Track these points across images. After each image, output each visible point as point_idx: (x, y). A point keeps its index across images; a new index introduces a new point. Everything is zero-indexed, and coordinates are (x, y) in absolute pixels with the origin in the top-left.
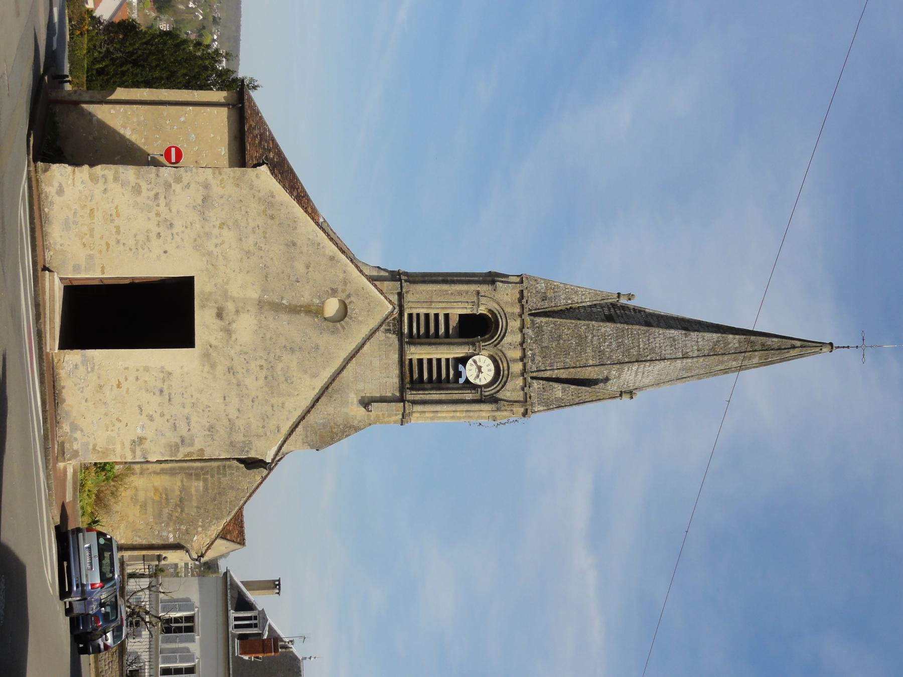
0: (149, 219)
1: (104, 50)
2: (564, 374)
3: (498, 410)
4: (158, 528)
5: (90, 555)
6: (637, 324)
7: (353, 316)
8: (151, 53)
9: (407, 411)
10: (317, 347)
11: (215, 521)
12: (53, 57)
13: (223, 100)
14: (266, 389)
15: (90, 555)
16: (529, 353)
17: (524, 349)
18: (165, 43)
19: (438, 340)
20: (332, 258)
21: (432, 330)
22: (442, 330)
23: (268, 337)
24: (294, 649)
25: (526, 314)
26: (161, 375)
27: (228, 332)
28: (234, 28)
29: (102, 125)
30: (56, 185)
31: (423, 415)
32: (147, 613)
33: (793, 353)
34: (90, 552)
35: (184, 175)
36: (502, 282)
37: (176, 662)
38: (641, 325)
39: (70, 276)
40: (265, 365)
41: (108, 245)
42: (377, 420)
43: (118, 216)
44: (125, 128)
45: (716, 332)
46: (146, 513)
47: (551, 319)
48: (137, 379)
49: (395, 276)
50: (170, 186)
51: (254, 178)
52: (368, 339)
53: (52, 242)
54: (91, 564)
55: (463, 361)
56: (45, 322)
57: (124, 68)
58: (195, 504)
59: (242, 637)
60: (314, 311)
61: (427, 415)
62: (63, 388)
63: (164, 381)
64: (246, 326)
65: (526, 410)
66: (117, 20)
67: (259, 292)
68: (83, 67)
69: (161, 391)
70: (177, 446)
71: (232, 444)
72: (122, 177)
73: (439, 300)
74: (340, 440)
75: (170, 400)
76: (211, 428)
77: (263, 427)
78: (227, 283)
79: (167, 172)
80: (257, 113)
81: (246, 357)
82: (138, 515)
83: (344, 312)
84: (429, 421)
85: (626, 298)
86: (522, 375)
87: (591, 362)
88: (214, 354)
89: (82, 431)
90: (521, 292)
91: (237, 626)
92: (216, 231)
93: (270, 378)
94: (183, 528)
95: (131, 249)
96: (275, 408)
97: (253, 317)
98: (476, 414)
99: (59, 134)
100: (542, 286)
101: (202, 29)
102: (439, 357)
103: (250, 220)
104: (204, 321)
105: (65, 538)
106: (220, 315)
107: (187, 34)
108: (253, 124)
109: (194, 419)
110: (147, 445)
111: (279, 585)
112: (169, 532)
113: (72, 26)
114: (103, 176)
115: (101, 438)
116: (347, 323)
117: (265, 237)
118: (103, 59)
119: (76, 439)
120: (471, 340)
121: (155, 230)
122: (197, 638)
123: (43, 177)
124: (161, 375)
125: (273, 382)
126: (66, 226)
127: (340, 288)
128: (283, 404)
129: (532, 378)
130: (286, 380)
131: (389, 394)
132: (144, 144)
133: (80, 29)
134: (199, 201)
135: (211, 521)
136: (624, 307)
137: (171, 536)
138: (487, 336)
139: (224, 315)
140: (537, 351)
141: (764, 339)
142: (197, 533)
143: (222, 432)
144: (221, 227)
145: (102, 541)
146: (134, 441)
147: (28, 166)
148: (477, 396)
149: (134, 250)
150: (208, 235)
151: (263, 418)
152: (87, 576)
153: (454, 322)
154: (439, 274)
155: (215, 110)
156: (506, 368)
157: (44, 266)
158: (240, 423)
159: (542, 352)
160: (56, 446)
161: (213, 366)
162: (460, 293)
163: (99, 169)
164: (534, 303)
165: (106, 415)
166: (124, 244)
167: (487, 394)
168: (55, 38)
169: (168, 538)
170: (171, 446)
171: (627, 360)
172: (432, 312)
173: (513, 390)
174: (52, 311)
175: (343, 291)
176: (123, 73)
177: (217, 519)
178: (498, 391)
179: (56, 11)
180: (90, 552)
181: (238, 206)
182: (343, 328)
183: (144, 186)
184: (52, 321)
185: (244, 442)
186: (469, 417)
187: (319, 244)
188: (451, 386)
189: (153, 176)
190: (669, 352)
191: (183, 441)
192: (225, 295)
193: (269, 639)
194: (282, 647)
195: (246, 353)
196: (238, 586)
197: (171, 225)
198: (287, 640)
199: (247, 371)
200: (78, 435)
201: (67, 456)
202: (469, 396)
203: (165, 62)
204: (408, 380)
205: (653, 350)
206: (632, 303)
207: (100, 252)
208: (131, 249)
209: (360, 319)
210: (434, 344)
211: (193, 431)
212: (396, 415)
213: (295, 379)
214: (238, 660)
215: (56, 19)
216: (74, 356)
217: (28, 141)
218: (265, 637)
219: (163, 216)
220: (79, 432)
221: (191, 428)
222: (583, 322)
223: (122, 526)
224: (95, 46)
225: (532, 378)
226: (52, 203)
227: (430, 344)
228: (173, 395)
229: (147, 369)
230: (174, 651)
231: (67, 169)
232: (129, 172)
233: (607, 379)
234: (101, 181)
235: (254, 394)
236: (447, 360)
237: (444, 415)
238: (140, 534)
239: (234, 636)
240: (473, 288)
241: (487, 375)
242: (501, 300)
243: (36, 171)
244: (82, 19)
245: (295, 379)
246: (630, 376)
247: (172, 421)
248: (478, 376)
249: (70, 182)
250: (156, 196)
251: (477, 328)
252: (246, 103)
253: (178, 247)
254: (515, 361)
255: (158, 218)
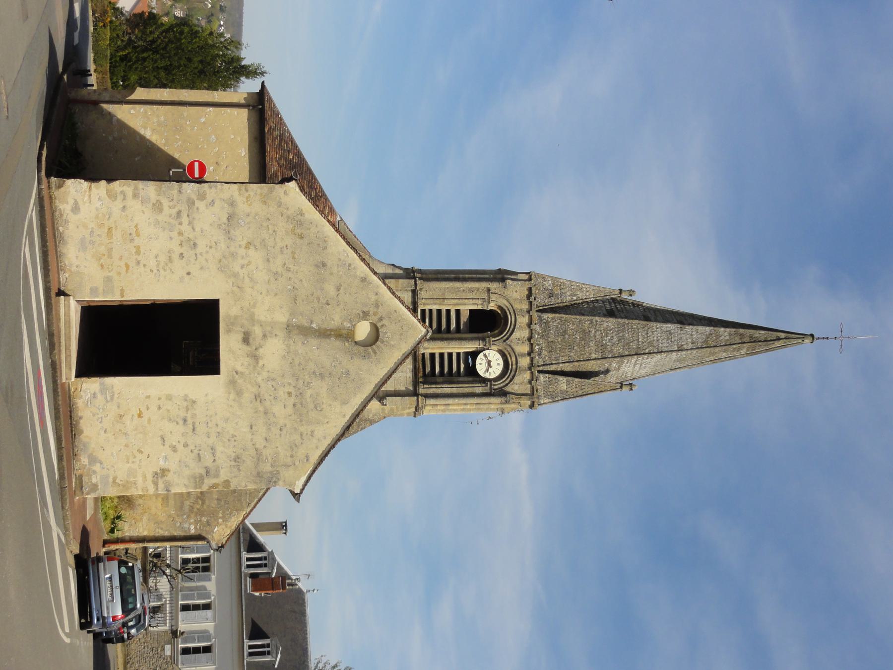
0: (171, 238)
1: (126, 38)
2: (568, 368)
3: (507, 402)
4: (180, 520)
5: (112, 586)
6: (636, 319)
7: (385, 339)
8: (170, 41)
9: (420, 405)
10: (348, 373)
11: (235, 512)
12: (74, 53)
13: (243, 101)
14: (294, 417)
15: (112, 586)
16: (536, 348)
17: (532, 345)
18: (181, 33)
19: (450, 336)
20: (364, 280)
21: (444, 326)
22: (453, 326)
23: (297, 362)
24: (300, 585)
25: (534, 310)
26: (185, 404)
27: (255, 358)
28: (237, 16)
29: (122, 125)
30: (71, 201)
31: (435, 408)
32: (168, 566)
33: (777, 344)
34: (111, 583)
35: (208, 191)
36: (512, 279)
37: (194, 599)
38: (640, 319)
39: (86, 299)
40: (293, 393)
41: (127, 266)
42: (392, 413)
43: (138, 235)
44: (146, 128)
45: (709, 325)
46: (167, 506)
47: (557, 315)
48: (159, 408)
49: (410, 274)
50: (193, 203)
51: (282, 194)
52: (401, 364)
53: (67, 263)
54: (112, 595)
55: (474, 355)
56: (60, 351)
57: (145, 55)
58: (215, 496)
59: (253, 576)
60: (345, 335)
61: (439, 407)
62: (81, 418)
63: (187, 410)
64: (273, 351)
65: (533, 403)
66: (138, 11)
67: (287, 316)
68: (106, 56)
69: (185, 421)
70: (201, 478)
71: (259, 475)
72: (142, 193)
73: (451, 296)
74: (355, 433)
75: (194, 430)
76: (237, 459)
77: (292, 456)
78: (254, 306)
79: (189, 188)
80: (278, 114)
81: (273, 383)
82: (160, 507)
83: (375, 336)
84: (440, 413)
85: (627, 294)
86: (530, 369)
87: (594, 356)
88: (240, 381)
89: (101, 463)
90: (530, 289)
91: (249, 566)
92: (242, 251)
93: (299, 405)
94: (204, 519)
95: (152, 271)
96: (304, 436)
97: (281, 342)
98: (486, 406)
99: (76, 144)
100: (549, 284)
101: (210, 18)
102: (450, 351)
103: (277, 240)
104: (229, 346)
105: (85, 565)
106: (246, 340)
107: (198, 20)
108: (273, 126)
109: (219, 449)
110: (170, 477)
111: (286, 526)
112: (190, 524)
113: (95, 18)
114: (122, 192)
115: (121, 471)
116: (379, 347)
117: (294, 258)
118: (125, 48)
119: (94, 472)
120: (480, 335)
121: (178, 250)
122: (213, 577)
123: (56, 193)
124: (185, 404)
125: (301, 408)
126: (83, 245)
127: (372, 310)
128: (312, 432)
129: (539, 372)
130: (316, 407)
131: (403, 388)
132: (165, 145)
133: (103, 21)
134: (225, 220)
135: (231, 513)
136: (623, 302)
137: (192, 527)
138: (496, 332)
139: (251, 341)
140: (544, 345)
141: (752, 331)
142: (218, 524)
143: (249, 463)
144: (247, 247)
145: (124, 570)
146: (156, 474)
147: (39, 183)
148: (486, 390)
149: (155, 271)
150: (233, 255)
151: (291, 447)
152: (108, 608)
153: (464, 317)
154: (452, 272)
155: (235, 111)
156: (514, 363)
157: (59, 290)
158: (268, 453)
159: (548, 346)
160: (74, 480)
161: (239, 393)
162: (471, 290)
163: (117, 185)
164: (541, 299)
165: (127, 446)
166: (144, 265)
167: (496, 387)
168: (76, 34)
169: (189, 529)
170: (195, 478)
171: (627, 353)
172: (444, 308)
173: (521, 384)
174: (68, 338)
175: (375, 314)
176: (144, 59)
177: (237, 510)
178: (507, 385)
179: (77, 7)
180: (111, 583)
181: (265, 224)
182: (375, 353)
183: (166, 203)
184: (68, 348)
185: (271, 472)
186: (479, 409)
187: (350, 265)
188: (461, 379)
189: (175, 192)
190: (665, 345)
191: (207, 472)
192: (252, 319)
193: (277, 577)
194: (289, 585)
195: (273, 380)
196: (249, 529)
197: (195, 244)
198: (294, 578)
199: (275, 398)
200: (97, 467)
201: (86, 490)
202: (479, 390)
203: (183, 50)
204: (421, 374)
205: (651, 344)
206: (635, 298)
207: (119, 274)
208: (152, 271)
209: (392, 343)
210: (447, 339)
211: (218, 462)
212: (410, 408)
213: (324, 406)
214: (250, 597)
215: (77, 14)
216: (92, 385)
217: (39, 161)
218: (273, 576)
219: (186, 235)
220: (98, 464)
221: (217, 458)
222: (587, 318)
223: (145, 518)
224: (118, 35)
225: (539, 372)
226: (66, 222)
227: (442, 339)
228: (197, 424)
229: (169, 398)
230: (191, 589)
231: (84, 184)
232: (149, 189)
233: (607, 371)
234: (120, 197)
235: (281, 422)
236: (458, 354)
237: (455, 407)
238: (161, 526)
239: (246, 575)
240: (484, 285)
241: (496, 369)
242: (510, 298)
243: (49, 187)
244: (105, 12)
245: (324, 406)
246: (629, 368)
247: (196, 452)
248: (487, 370)
249: (86, 198)
250: (179, 213)
251: (487, 323)
252: (266, 104)
253: (202, 268)
254: (523, 355)
255: (181, 238)
